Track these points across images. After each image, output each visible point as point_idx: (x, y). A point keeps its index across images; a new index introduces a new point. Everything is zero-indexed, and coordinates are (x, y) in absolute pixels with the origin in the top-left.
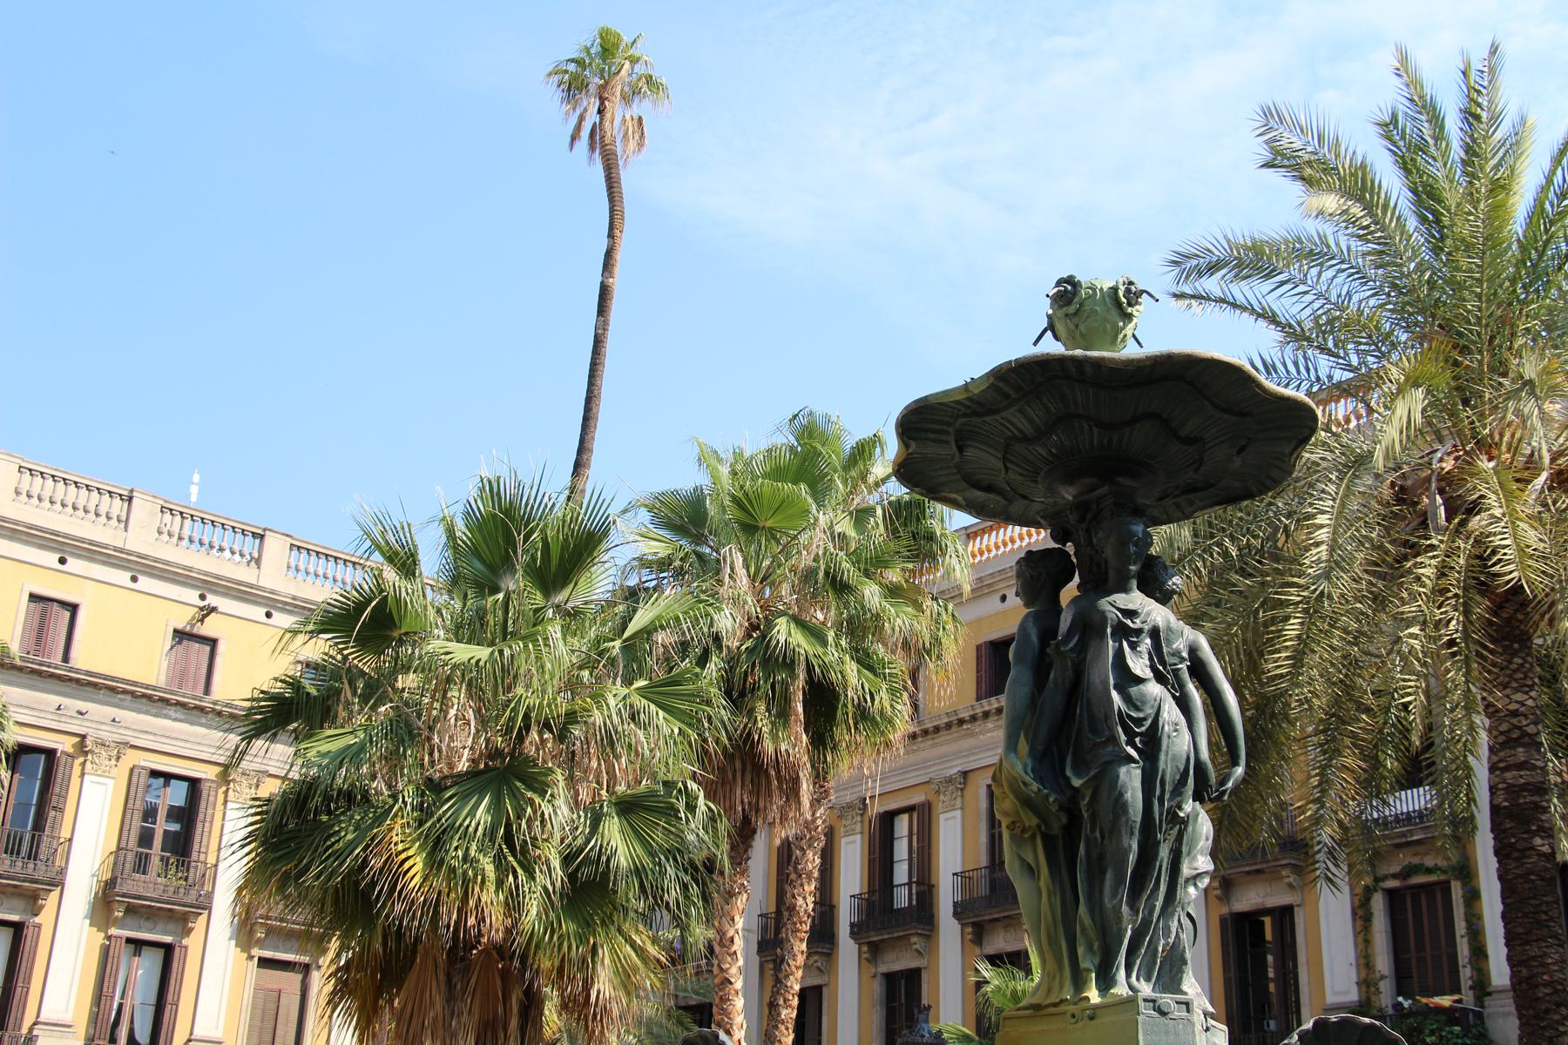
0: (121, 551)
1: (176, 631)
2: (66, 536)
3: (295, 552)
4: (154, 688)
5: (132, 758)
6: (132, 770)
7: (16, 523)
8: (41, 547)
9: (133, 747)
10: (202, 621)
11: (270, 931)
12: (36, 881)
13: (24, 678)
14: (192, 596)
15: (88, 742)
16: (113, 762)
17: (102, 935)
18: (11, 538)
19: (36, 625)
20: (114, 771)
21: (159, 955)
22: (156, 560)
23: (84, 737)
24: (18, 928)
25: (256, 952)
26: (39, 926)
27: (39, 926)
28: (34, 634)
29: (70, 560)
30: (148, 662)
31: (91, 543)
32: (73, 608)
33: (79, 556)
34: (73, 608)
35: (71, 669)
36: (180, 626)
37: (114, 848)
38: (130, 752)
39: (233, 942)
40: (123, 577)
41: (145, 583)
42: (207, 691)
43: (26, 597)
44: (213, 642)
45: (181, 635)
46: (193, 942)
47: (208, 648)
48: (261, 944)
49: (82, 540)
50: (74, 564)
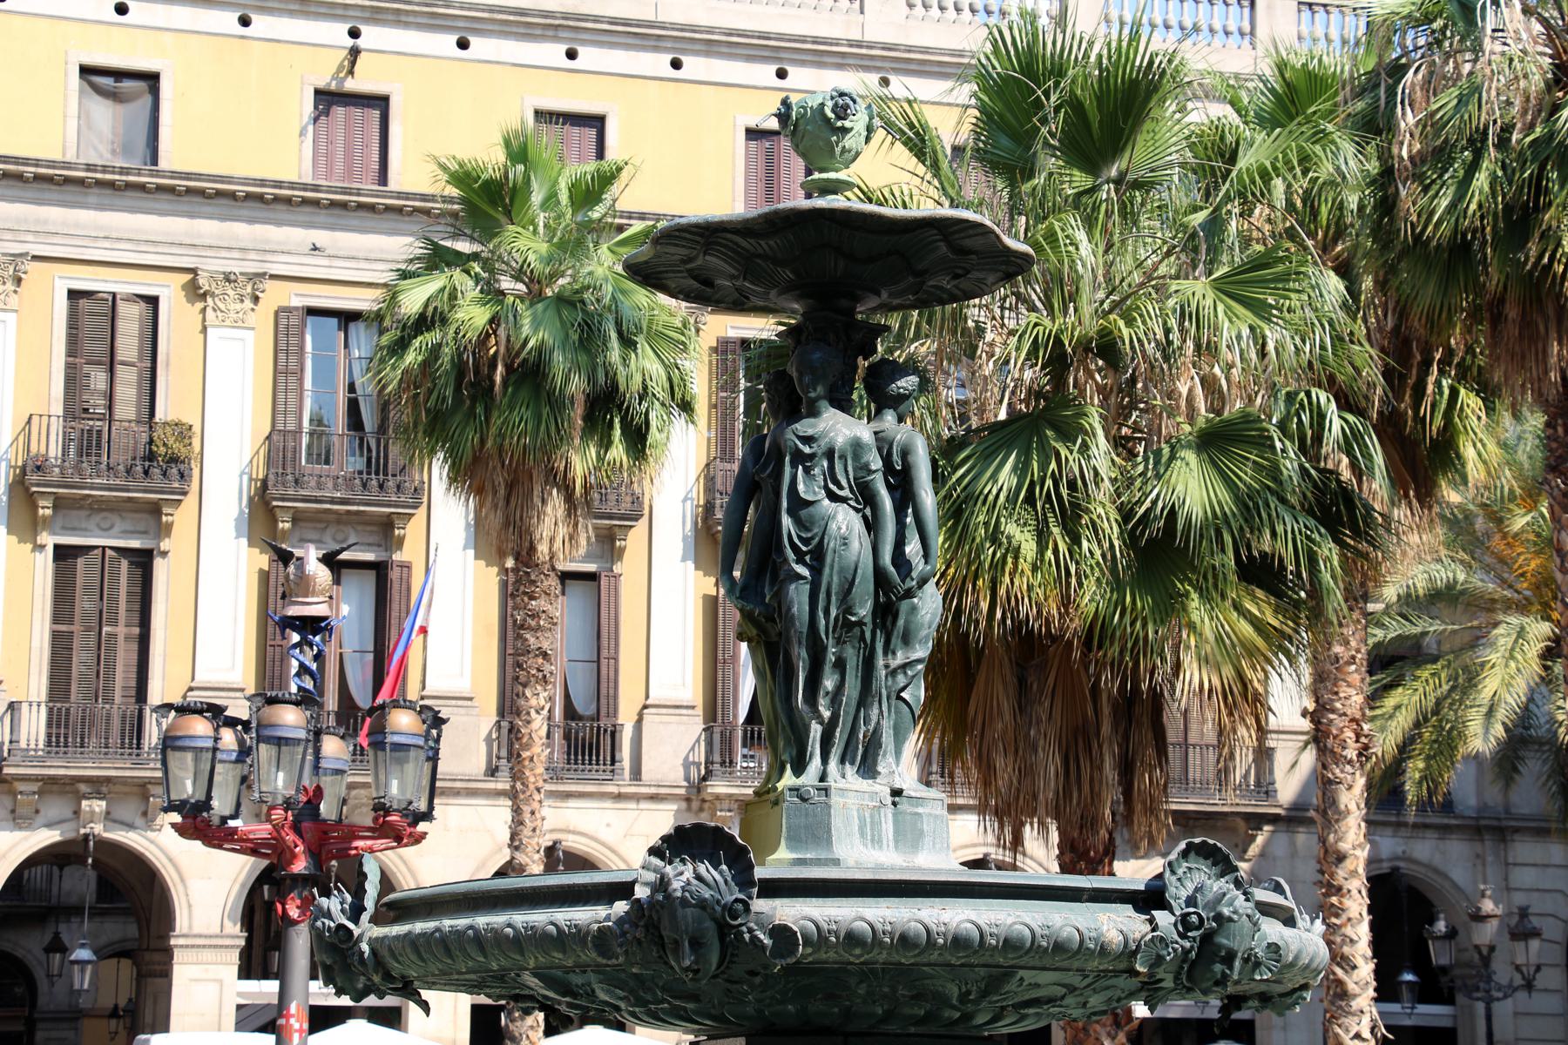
0: (859, 44)
1: (318, 92)
2: (780, 37)
3: (1306, 14)
4: (292, 185)
5: (277, 295)
6: (276, 313)
7: (710, 30)
8: (750, 58)
9: (273, 277)
10: (351, 72)
11: (59, 503)
12: (610, 517)
13: (94, 196)
14: (764, 73)
15: (203, 281)
16: (248, 304)
17: (495, 569)
18: (708, 54)
19: (762, 173)
20: (252, 319)
21: (370, 577)
22: (909, 49)
23: (194, 271)
24: (380, 569)
25: (49, 540)
26: (407, 567)
27: (407, 567)
28: (761, 185)
29: (582, 51)
30: (286, 152)
31: (816, 40)
32: (152, 79)
33: (803, 63)
34: (152, 79)
35: (158, 174)
36: (321, 84)
37: (268, 429)
38: (269, 285)
39: (691, 565)
40: (658, 63)
41: (694, 66)
42: (383, 177)
43: (741, 135)
44: (380, 102)
45: (327, 99)
46: (177, 545)
47: (593, 133)
48: (47, 524)
49: (802, 39)
50: (589, 56)
